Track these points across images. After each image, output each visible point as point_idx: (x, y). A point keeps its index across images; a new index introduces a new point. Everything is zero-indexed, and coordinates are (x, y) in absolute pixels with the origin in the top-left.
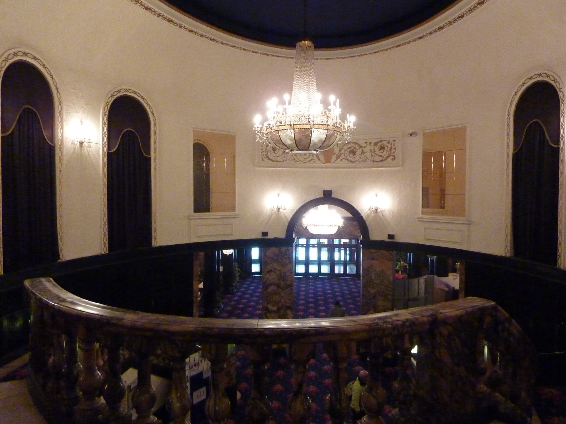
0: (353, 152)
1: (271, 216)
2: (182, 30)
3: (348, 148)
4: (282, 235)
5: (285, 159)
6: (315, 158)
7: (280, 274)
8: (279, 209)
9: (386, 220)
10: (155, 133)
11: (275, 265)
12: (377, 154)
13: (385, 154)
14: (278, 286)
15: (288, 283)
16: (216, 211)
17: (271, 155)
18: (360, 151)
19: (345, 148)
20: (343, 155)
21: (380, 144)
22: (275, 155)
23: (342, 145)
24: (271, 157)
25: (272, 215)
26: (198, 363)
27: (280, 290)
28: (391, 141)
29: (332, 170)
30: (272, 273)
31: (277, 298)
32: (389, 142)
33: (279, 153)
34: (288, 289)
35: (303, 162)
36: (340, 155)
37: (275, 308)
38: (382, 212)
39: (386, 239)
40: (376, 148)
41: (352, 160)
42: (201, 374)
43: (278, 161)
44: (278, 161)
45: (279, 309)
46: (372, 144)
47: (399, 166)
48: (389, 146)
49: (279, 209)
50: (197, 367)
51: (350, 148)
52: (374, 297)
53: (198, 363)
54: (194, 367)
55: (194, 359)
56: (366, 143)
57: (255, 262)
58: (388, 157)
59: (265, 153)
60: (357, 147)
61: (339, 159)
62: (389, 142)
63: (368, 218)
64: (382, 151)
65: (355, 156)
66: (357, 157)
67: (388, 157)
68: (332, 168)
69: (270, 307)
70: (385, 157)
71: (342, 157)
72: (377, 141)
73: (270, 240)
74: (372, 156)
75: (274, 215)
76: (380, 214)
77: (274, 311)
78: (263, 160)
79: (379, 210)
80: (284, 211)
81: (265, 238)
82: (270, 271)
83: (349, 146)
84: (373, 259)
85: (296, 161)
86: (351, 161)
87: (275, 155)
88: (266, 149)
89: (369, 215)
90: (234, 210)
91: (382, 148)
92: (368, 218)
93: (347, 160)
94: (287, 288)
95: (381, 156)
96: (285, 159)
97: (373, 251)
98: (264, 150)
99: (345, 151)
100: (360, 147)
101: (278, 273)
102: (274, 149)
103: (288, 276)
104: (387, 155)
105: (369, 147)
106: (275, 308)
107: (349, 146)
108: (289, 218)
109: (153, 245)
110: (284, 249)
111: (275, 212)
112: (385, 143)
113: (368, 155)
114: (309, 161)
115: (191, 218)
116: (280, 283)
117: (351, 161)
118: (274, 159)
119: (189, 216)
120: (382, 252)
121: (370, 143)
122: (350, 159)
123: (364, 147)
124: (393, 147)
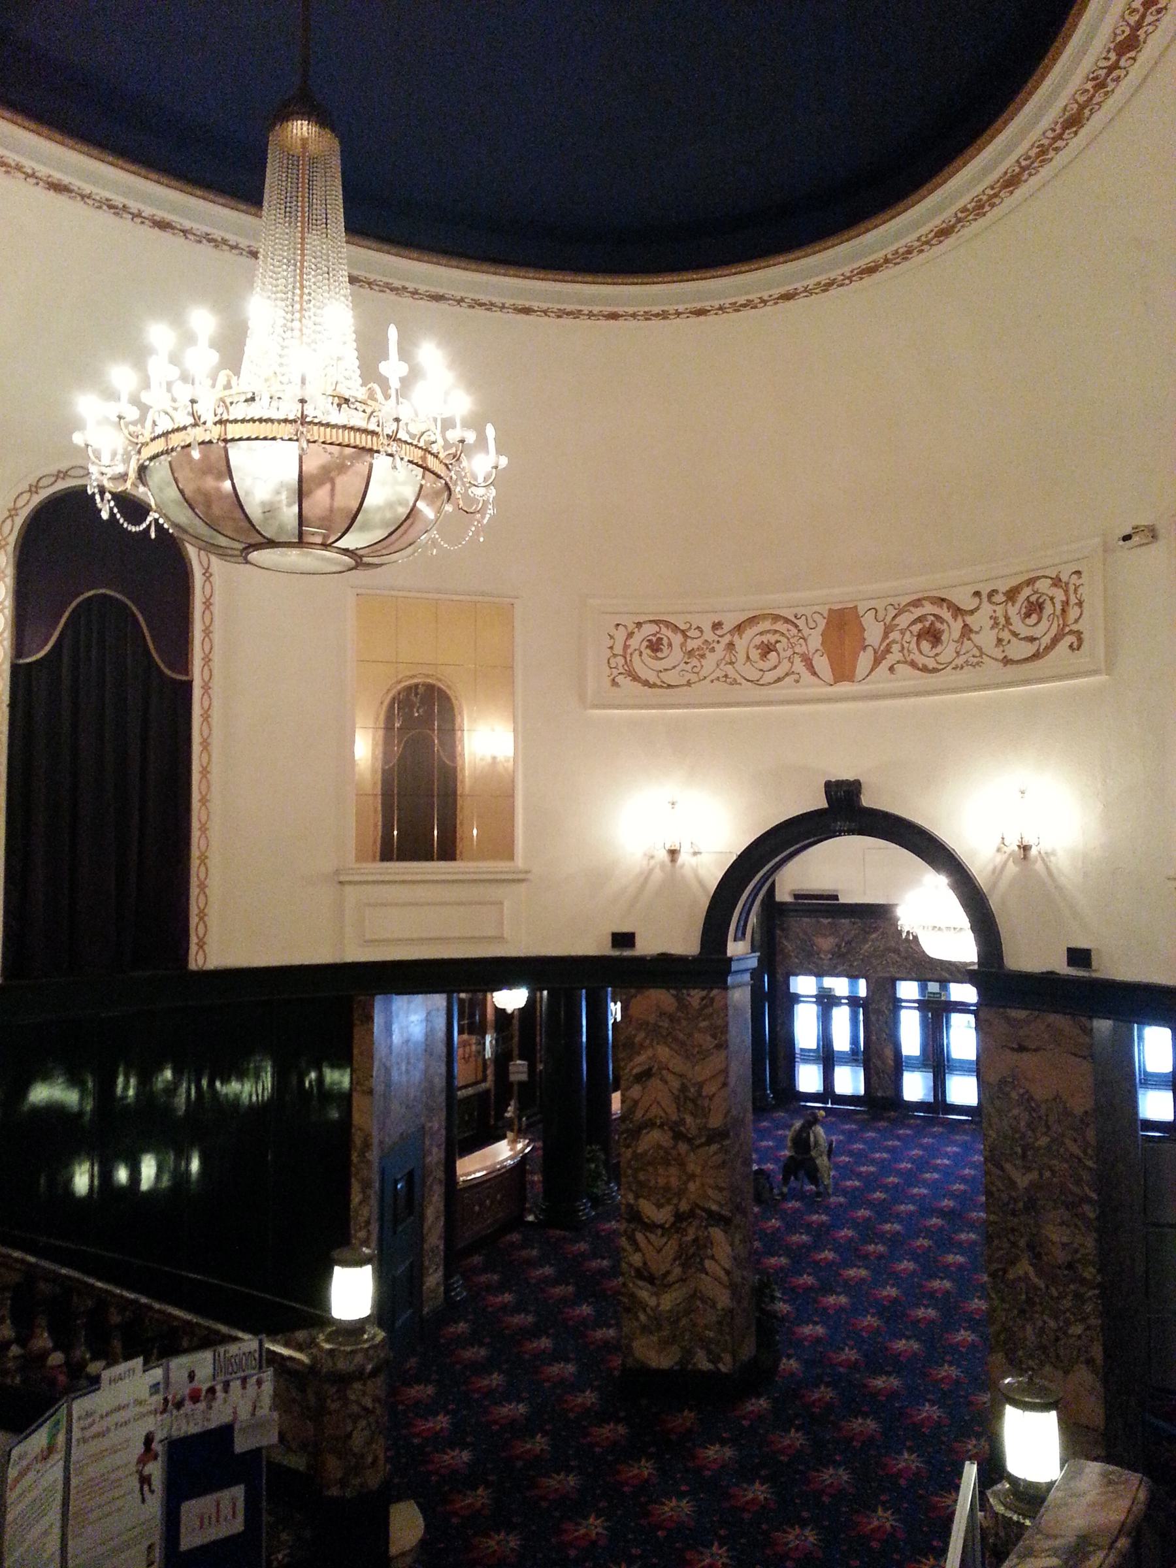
0: (933, 635)
1: (647, 876)
2: (126, 223)
3: (914, 623)
4: (683, 941)
5: (694, 678)
6: (799, 666)
7: (684, 1088)
8: (673, 853)
9: (1059, 888)
10: (207, 632)
11: (663, 1052)
12: (1015, 635)
13: (1044, 629)
14: (678, 1136)
15: (715, 1122)
16: (472, 859)
17: (645, 666)
18: (957, 626)
19: (904, 620)
20: (895, 648)
21: (1026, 592)
22: (660, 665)
23: (892, 612)
24: (644, 673)
25: (651, 871)
26: (212, 1391)
27: (683, 1147)
28: (1064, 578)
29: (860, 705)
30: (655, 1082)
31: (671, 1176)
32: (1057, 582)
33: (675, 656)
34: (714, 1147)
35: (755, 682)
36: (888, 651)
37: (663, 1216)
38: (1044, 858)
39: (1061, 966)
40: (1013, 611)
41: (931, 664)
42: (225, 1432)
43: (669, 686)
44: (669, 686)
45: (679, 1217)
46: (1000, 598)
47: (1095, 672)
48: (1059, 595)
49: (673, 853)
50: (202, 1406)
51: (920, 619)
52: (1031, 1205)
53: (212, 1391)
54: (188, 1406)
55: (192, 1376)
56: (977, 594)
57: (962, 1067)
58: (1055, 641)
59: (621, 661)
60: (946, 614)
61: (885, 664)
62: (1057, 582)
63: (994, 885)
64: (1034, 617)
65: (939, 649)
66: (947, 651)
67: (1055, 641)
68: (854, 698)
69: (648, 1209)
70: (1046, 641)
71: (891, 659)
72: (1014, 582)
73: (641, 960)
74: (1000, 641)
75: (658, 875)
76: (1039, 866)
77: (661, 1226)
78: (614, 683)
79: (1034, 852)
80: (693, 861)
81: (627, 953)
82: (645, 1075)
83: (918, 612)
84: (1022, 1049)
85: (735, 682)
86: (925, 669)
87: (660, 665)
88: (626, 647)
89: (998, 872)
90: (511, 857)
91: (1035, 608)
92: (994, 885)
93: (913, 664)
94: (709, 1142)
95: (1032, 639)
96: (694, 678)
97: (1021, 1014)
98: (618, 649)
99: (903, 632)
100: (957, 611)
101: (675, 1084)
102: (655, 646)
103: (711, 1098)
104: (1054, 631)
105: (987, 608)
106: (663, 1216)
107: (918, 612)
108: (713, 883)
109: (192, 966)
110: (695, 996)
111: (662, 865)
112: (1043, 586)
113: (986, 638)
114: (779, 680)
115: (342, 878)
116: (682, 1121)
117: (925, 669)
118: (652, 679)
119: (337, 872)
120: (1052, 1018)
121: (993, 593)
122: (921, 660)
123: (972, 612)
124: (1073, 600)
